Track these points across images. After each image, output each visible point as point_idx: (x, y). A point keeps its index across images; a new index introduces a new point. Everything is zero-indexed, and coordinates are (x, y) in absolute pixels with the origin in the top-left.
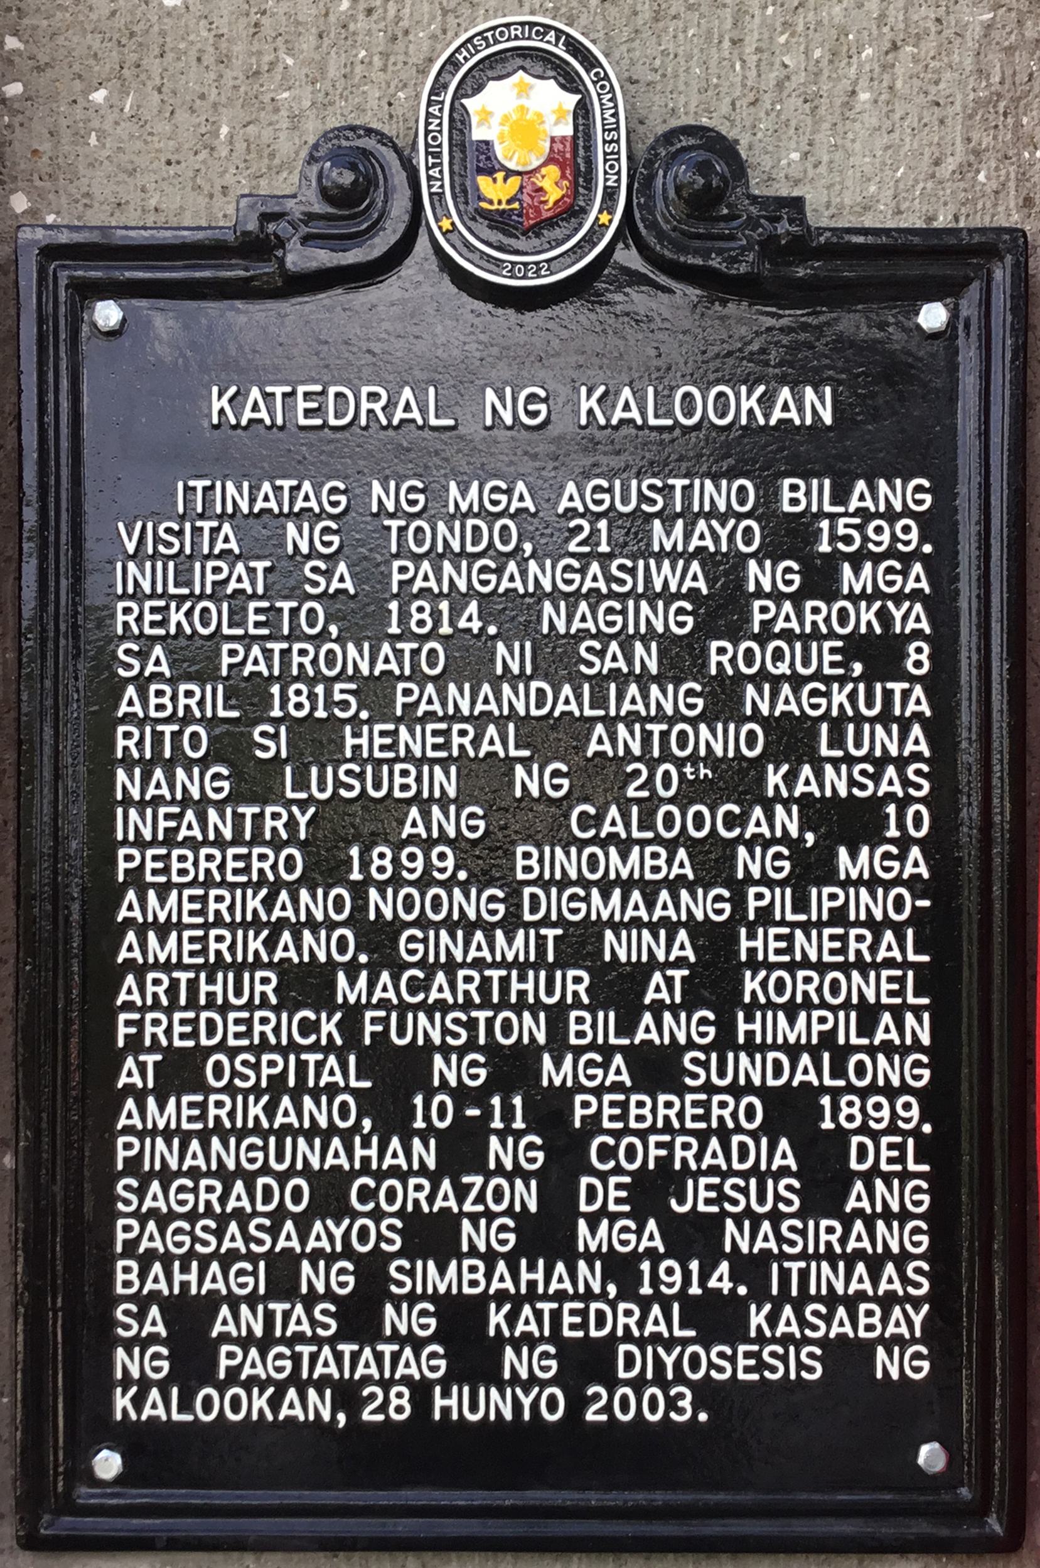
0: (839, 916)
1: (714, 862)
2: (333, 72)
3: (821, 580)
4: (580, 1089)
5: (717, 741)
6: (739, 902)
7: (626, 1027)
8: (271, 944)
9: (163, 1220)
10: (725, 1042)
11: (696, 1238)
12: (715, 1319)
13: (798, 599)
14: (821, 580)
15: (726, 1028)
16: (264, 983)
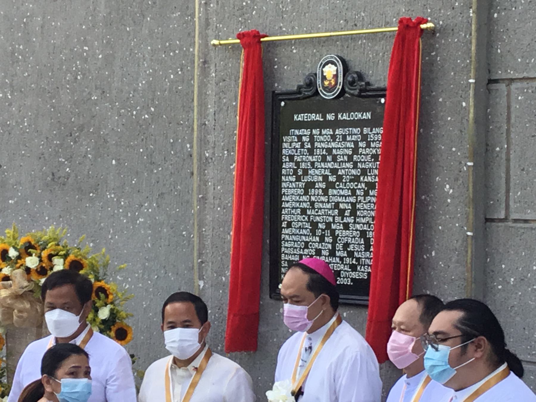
0: (370, 202)
1: (354, 192)
2: (313, 61)
3: (368, 146)
4: (336, 229)
5: (354, 172)
6: (357, 199)
7: (342, 220)
8: (300, 205)
9: (287, 248)
10: (355, 223)
11: (351, 254)
12: (353, 268)
13: (365, 148)
14: (368, 146)
15: (355, 219)
16: (299, 211)
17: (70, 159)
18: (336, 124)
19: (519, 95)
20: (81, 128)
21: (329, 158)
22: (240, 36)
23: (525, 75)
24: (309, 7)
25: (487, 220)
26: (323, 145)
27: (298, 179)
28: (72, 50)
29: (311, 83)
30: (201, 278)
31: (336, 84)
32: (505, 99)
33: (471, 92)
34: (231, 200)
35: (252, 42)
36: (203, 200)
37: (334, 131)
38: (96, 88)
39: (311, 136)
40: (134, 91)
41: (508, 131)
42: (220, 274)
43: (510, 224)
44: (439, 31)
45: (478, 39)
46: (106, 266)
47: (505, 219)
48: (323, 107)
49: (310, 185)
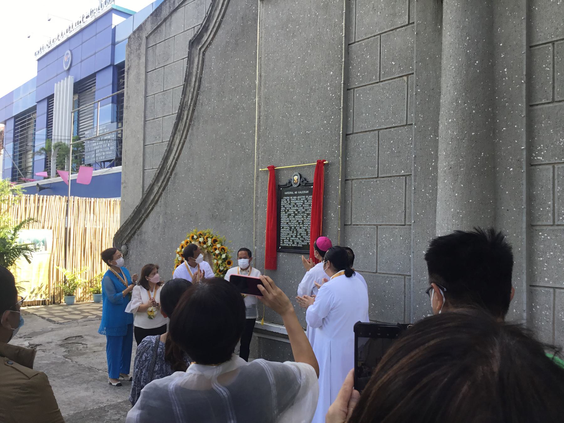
1: (303, 216)
17: (218, 210)
18: (297, 195)
19: (355, 184)
20: (222, 200)
22: (268, 168)
27: (286, 213)
29: (290, 182)
30: (256, 245)
34: (265, 220)
35: (272, 169)
36: (257, 220)
39: (290, 199)
41: (352, 196)
42: (262, 244)
48: (294, 190)
49: (290, 215)
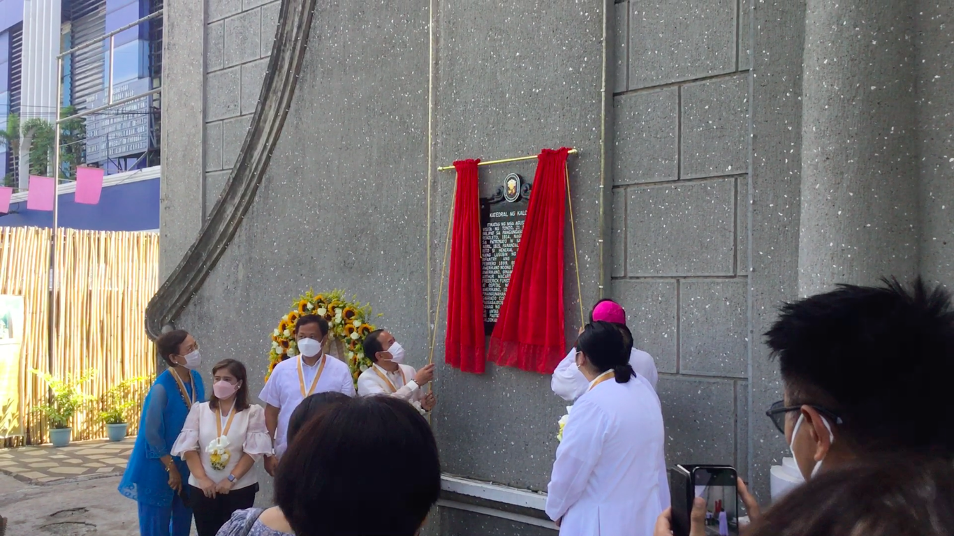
16: (493, 276)
20: (362, 231)
21: (512, 241)
22: (455, 164)
23: (636, 181)
24: (499, 144)
25: (613, 278)
26: (508, 233)
28: (356, 182)
31: (515, 193)
32: (623, 198)
33: (601, 194)
37: (515, 223)
38: (372, 205)
39: (501, 227)
40: (395, 206)
41: (626, 219)
43: (628, 280)
44: (581, 155)
45: (605, 159)
46: (369, 314)
47: (624, 277)
48: (508, 208)
49: (500, 259)
